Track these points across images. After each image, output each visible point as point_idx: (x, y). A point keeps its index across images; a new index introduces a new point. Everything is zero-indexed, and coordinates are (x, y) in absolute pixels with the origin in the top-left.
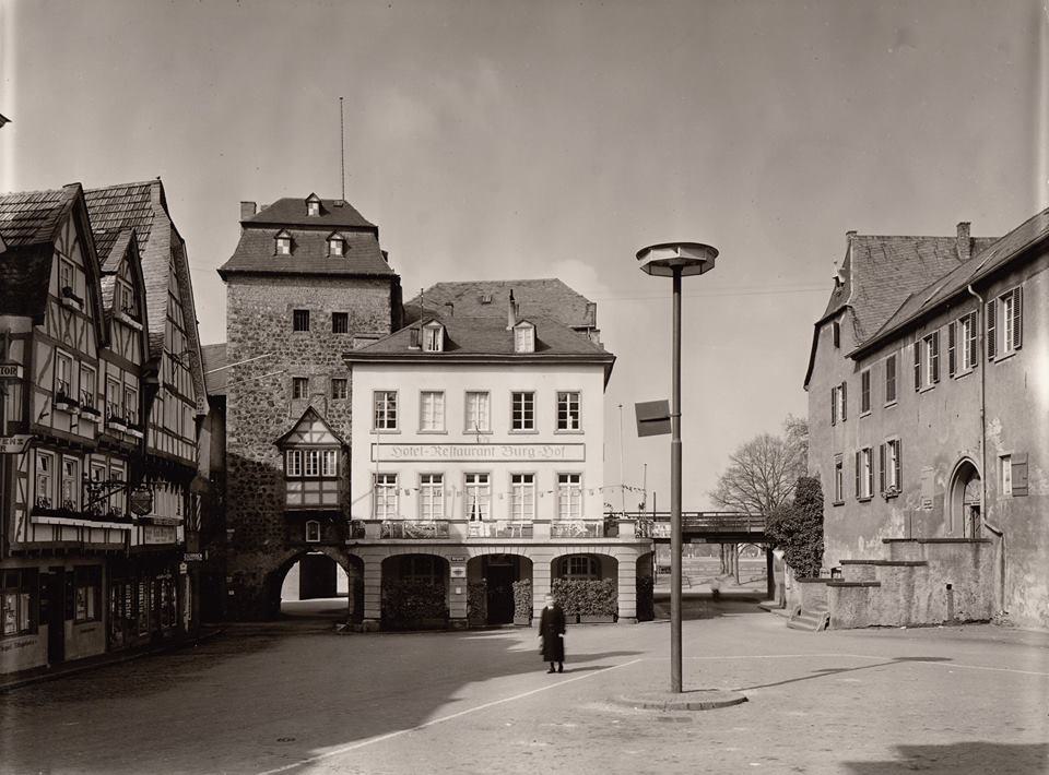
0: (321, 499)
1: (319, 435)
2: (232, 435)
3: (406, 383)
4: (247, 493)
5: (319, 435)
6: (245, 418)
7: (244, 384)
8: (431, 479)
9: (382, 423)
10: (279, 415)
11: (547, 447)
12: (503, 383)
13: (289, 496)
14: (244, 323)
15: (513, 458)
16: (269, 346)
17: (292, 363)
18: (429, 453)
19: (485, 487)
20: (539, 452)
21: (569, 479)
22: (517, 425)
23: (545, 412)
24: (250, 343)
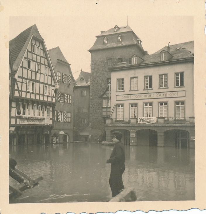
3: (125, 75)
4: (95, 112)
6: (95, 91)
8: (163, 104)
9: (161, 86)
11: (171, 93)
12: (141, 74)
13: (103, 113)
14: (95, 64)
15: (160, 97)
16: (101, 70)
18: (133, 97)
19: (120, 109)
20: (169, 95)
22: (177, 85)
23: (172, 80)
24: (96, 70)
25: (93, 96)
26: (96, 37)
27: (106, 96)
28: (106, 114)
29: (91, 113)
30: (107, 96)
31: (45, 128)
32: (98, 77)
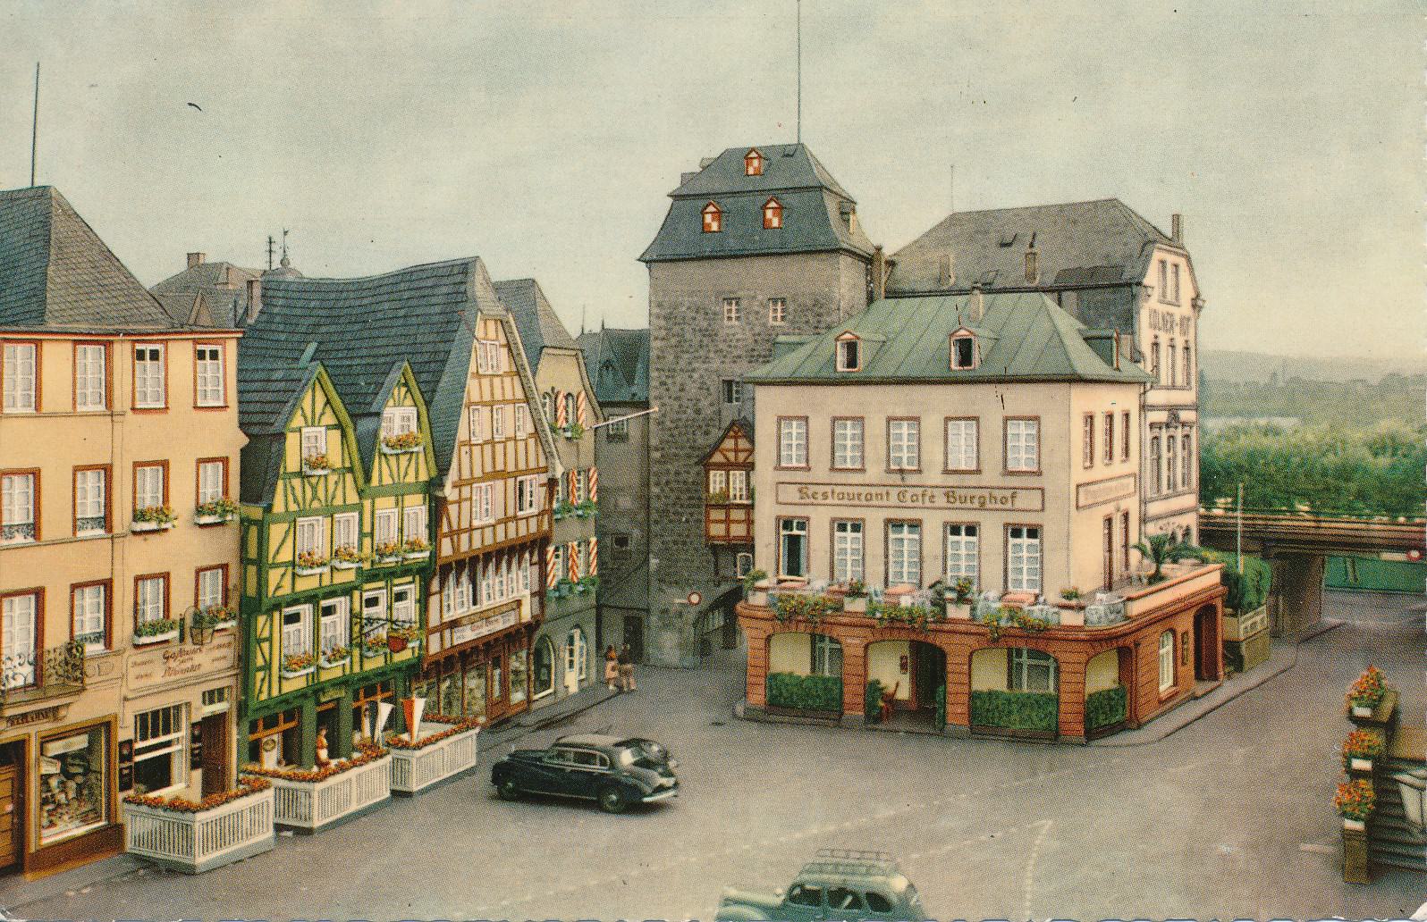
0: (728, 530)
1: (746, 454)
2: (657, 450)
5: (746, 454)
7: (668, 390)
8: (963, 528)
10: (708, 425)
16: (696, 342)
17: (723, 362)
21: (849, 528)
24: (673, 341)
25: (663, 449)
26: (669, 196)
27: (723, 460)
28: (722, 533)
29: (656, 522)
30: (726, 458)
31: (522, 633)
32: (682, 370)
